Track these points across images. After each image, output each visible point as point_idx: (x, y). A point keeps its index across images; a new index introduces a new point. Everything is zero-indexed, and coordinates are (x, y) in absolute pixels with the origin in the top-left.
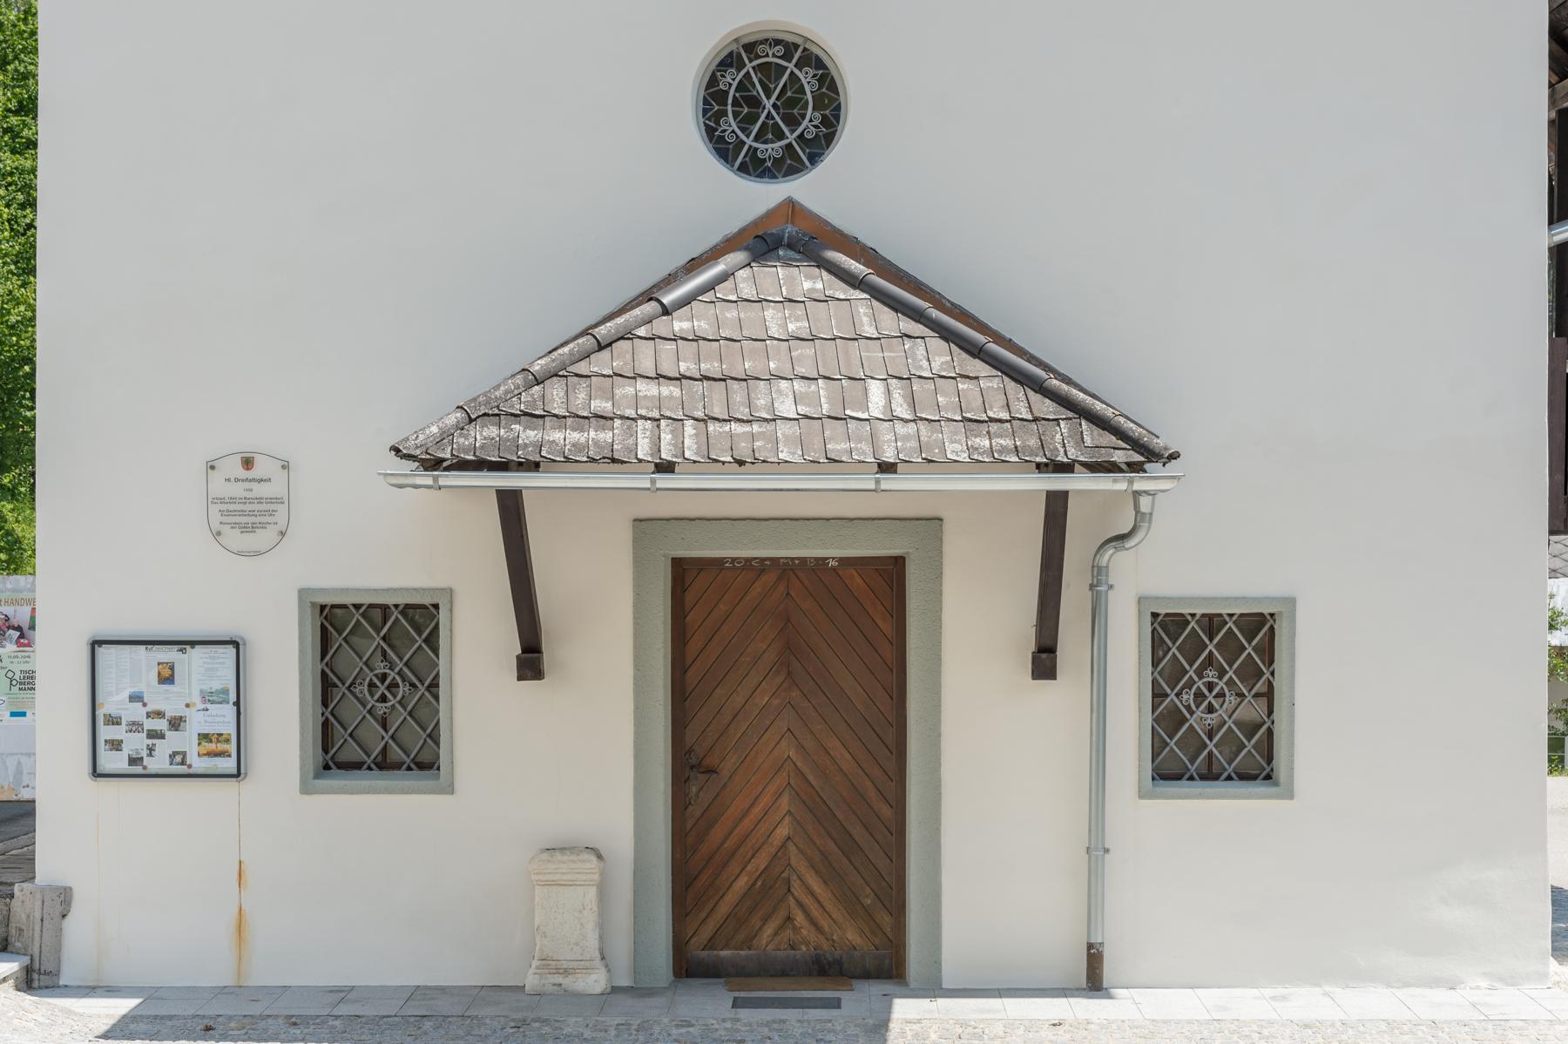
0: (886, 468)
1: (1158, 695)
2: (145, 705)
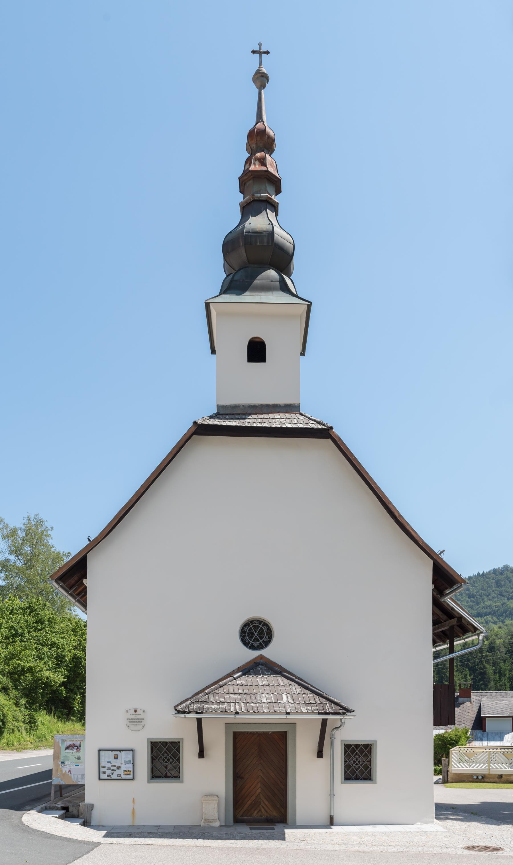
0: (288, 713)
1: (345, 761)
2: (111, 764)
